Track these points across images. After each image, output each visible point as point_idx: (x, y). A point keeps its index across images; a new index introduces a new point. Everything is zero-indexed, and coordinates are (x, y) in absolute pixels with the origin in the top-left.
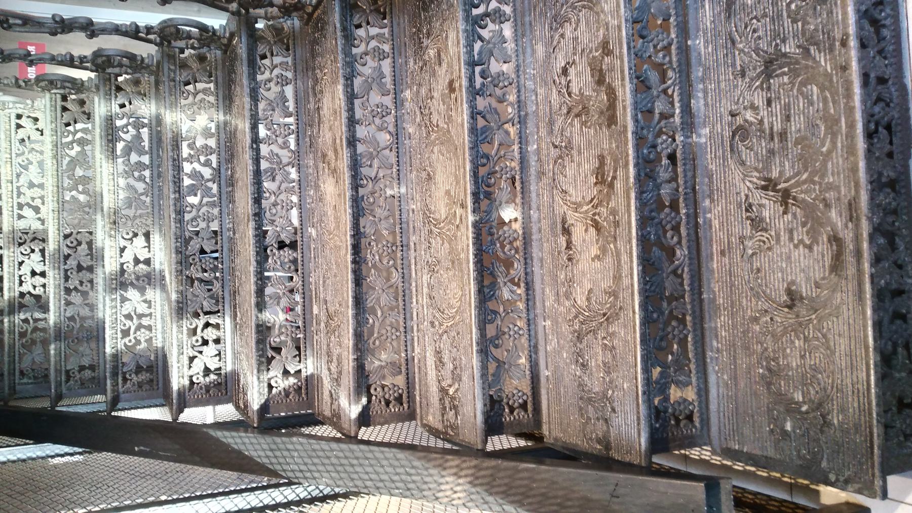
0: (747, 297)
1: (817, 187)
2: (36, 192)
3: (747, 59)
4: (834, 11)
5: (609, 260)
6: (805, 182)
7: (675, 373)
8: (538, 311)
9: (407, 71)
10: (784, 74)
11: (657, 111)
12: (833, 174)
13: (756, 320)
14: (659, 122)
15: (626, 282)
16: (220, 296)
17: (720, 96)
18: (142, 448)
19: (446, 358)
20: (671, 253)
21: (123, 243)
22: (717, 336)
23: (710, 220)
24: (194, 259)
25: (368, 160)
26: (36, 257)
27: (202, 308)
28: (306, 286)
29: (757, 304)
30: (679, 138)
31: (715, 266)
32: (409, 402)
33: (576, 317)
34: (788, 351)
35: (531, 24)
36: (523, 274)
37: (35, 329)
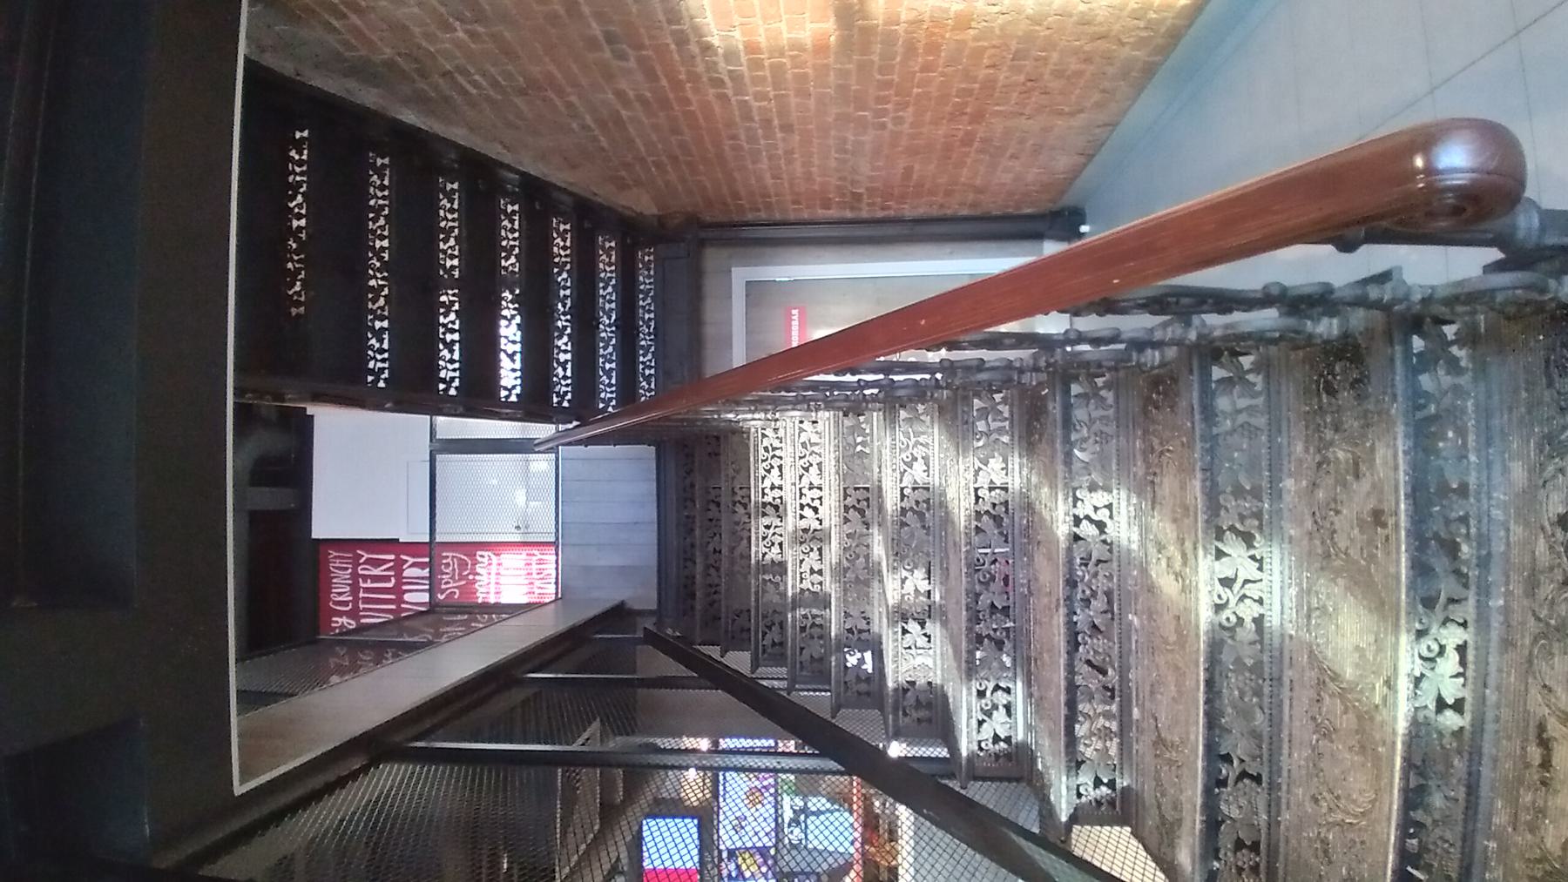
2: (816, 493)
21: (905, 574)
26: (814, 555)
37: (813, 625)
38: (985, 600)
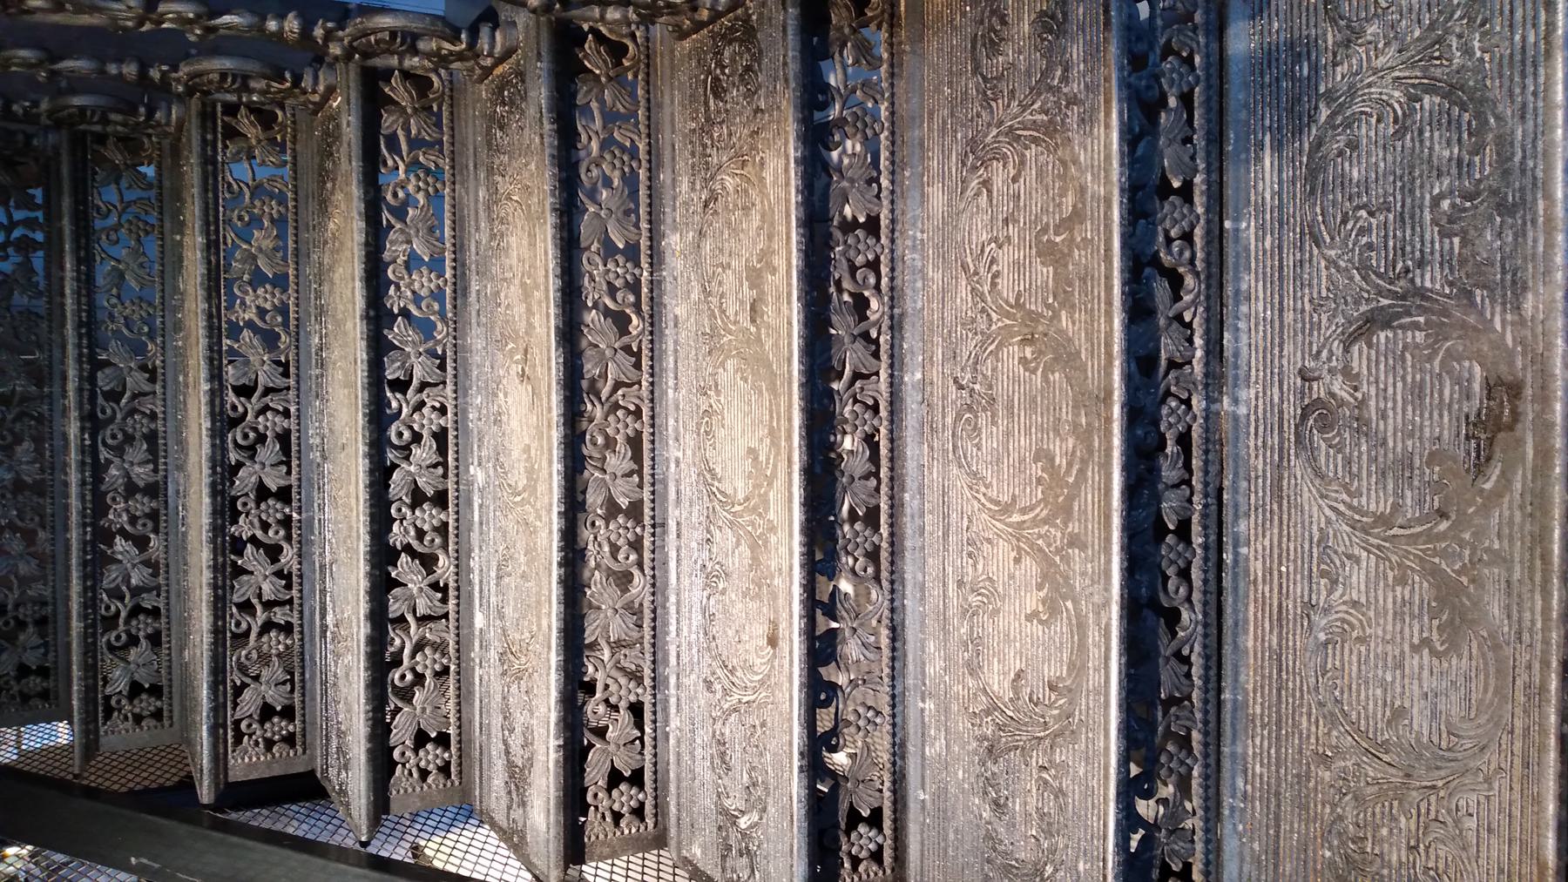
0: (1309, 715)
1: (1467, 552)
3: (1342, 281)
4: (1530, 234)
5: (1061, 627)
6: (1442, 537)
7: (1168, 837)
8: (910, 681)
9: (674, 199)
10: (1416, 326)
11: (1163, 355)
12: (1499, 536)
13: (1325, 760)
14: (1167, 374)
15: (1094, 679)
16: (295, 572)
17: (1281, 338)
18: (145, 861)
19: (735, 757)
20: (1173, 617)
22: (1245, 771)
23: (1247, 559)
24: (245, 504)
25: (596, 365)
27: (260, 596)
28: (463, 574)
29: (1329, 734)
30: (1198, 403)
31: (1250, 644)
32: (656, 815)
33: (988, 713)
34: (1385, 832)
35: (922, 145)
36: (887, 613)
38: (245, 480)
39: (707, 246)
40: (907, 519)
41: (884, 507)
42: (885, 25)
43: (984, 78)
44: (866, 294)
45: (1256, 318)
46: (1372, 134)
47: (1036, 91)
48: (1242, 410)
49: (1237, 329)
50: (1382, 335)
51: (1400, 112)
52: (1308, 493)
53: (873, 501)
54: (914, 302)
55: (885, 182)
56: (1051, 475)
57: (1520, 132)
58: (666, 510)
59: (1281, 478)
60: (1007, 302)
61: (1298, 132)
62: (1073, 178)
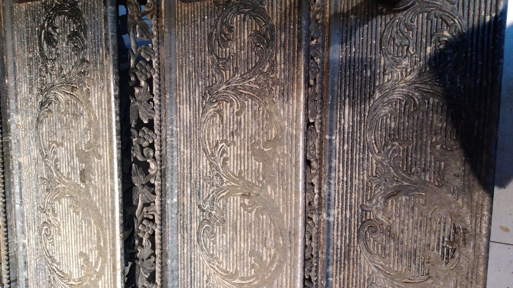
9: (16, 95)
39: (44, 129)
40: (169, 273)
41: (158, 269)
42: (155, 16)
43: (218, 57)
44: (148, 161)
45: (339, 179)
46: (402, 109)
47: (252, 72)
48: (331, 219)
49: (330, 184)
50: (404, 198)
51: (418, 103)
52: (364, 258)
53: (153, 268)
54: (173, 163)
55: (156, 101)
56: (261, 265)
57: (477, 123)
58: (16, 273)
59: (349, 251)
60: (233, 174)
61: (364, 100)
62: (276, 122)
